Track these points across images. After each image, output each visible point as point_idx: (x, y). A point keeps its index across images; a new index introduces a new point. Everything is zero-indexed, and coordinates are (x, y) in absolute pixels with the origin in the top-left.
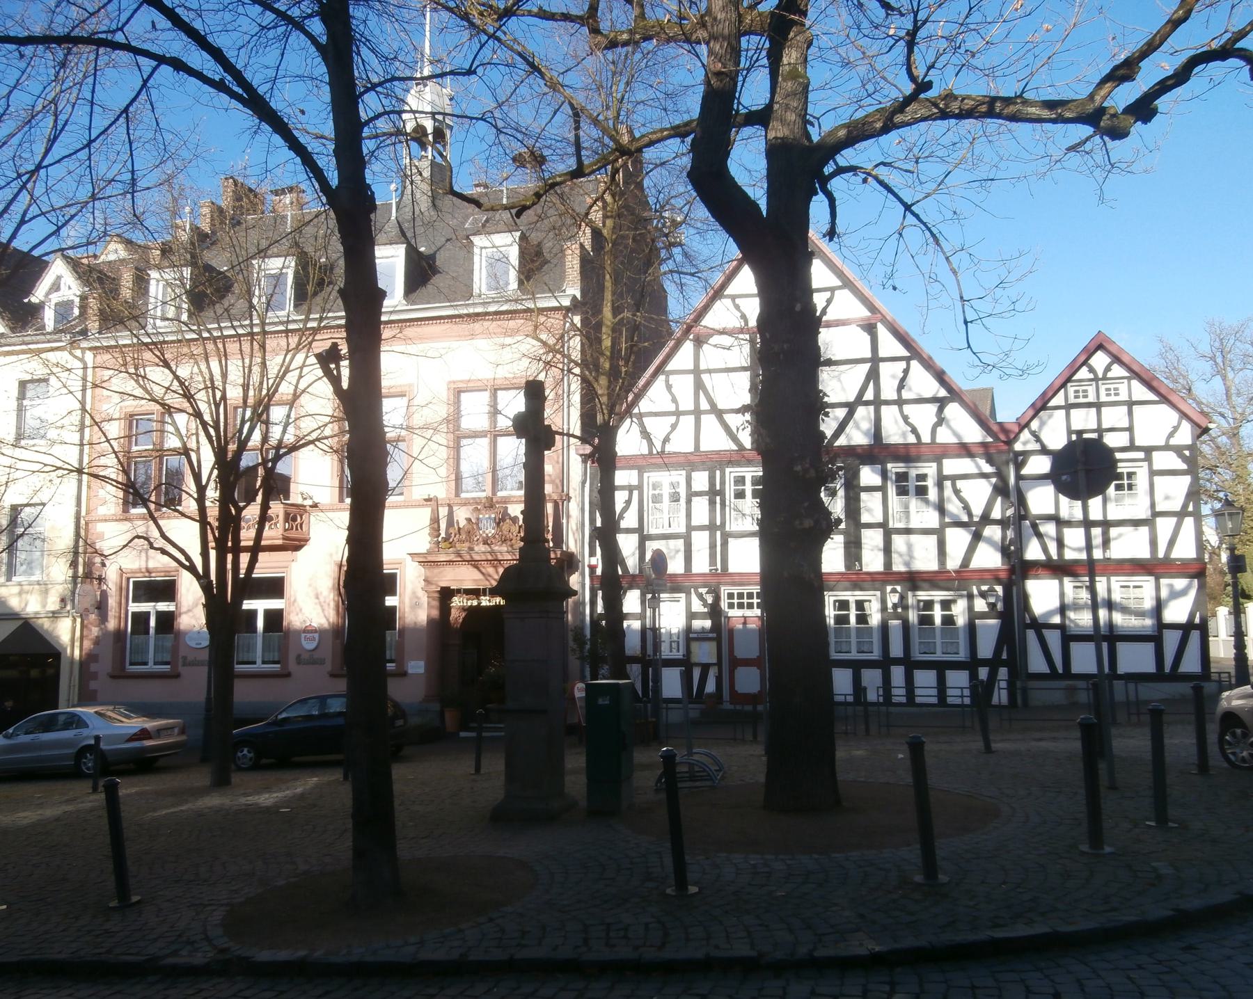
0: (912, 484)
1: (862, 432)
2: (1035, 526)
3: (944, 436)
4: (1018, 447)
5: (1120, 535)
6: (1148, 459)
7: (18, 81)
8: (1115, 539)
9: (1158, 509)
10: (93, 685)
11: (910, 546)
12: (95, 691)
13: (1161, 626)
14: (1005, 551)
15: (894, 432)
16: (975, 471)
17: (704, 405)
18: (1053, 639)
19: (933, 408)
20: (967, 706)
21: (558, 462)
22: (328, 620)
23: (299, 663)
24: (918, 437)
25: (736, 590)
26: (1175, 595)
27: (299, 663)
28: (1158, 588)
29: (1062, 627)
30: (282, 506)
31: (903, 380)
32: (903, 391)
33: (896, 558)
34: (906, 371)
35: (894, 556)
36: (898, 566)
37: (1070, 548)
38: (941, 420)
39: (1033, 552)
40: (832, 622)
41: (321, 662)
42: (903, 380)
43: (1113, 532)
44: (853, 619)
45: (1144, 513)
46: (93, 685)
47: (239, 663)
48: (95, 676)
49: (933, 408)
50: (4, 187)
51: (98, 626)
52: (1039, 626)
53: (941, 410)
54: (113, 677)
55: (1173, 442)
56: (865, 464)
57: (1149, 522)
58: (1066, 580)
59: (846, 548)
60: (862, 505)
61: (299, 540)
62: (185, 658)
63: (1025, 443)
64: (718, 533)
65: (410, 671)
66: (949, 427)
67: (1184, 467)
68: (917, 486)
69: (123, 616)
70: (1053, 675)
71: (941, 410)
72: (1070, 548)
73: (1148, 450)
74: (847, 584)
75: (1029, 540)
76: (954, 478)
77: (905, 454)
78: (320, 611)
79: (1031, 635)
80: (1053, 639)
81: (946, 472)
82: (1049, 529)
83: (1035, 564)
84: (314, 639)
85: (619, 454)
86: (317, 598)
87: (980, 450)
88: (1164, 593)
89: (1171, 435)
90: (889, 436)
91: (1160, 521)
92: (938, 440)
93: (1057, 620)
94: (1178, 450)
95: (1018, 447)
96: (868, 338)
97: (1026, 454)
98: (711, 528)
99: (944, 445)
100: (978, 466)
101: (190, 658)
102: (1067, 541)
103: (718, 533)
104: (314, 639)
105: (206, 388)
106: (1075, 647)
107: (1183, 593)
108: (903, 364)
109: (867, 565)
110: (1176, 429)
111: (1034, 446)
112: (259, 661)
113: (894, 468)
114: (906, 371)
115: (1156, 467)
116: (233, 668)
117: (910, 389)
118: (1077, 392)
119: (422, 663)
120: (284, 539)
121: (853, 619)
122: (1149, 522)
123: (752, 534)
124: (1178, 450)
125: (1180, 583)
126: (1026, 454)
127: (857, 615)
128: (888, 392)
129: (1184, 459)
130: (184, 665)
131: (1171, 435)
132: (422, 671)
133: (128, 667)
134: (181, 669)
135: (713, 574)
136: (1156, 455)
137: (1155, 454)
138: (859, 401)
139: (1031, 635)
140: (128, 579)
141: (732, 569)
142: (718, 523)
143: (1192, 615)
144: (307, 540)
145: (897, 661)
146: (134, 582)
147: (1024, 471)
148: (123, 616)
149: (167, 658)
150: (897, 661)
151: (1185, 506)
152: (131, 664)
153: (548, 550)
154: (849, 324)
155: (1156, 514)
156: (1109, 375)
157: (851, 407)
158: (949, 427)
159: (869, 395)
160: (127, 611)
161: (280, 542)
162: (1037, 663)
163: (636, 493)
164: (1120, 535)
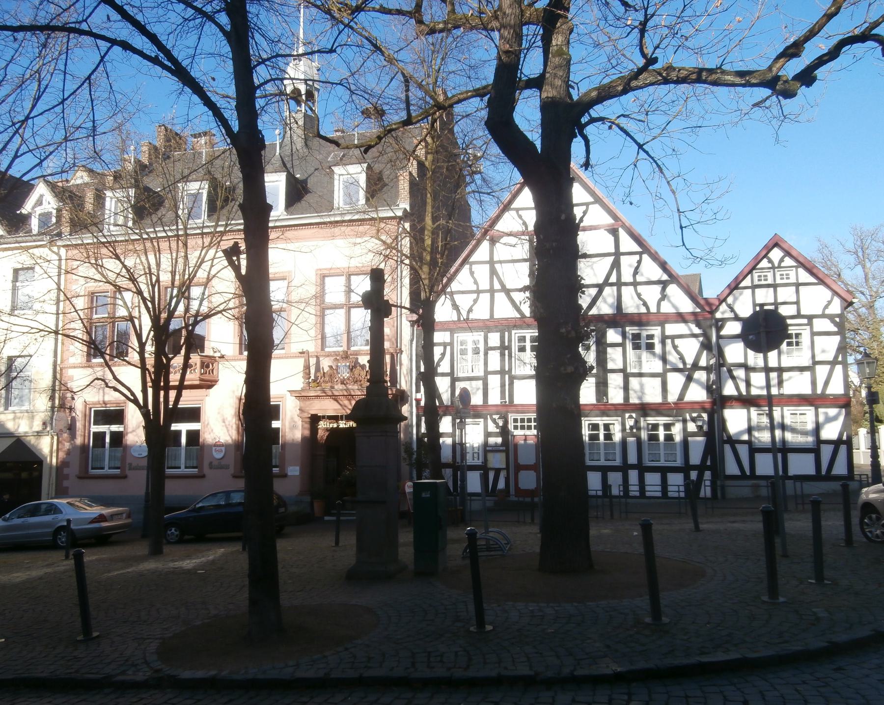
0: (643, 341)
1: (608, 305)
2: (730, 371)
3: (666, 308)
4: (718, 315)
5: (790, 378)
6: (810, 324)
7: (13, 57)
8: (787, 380)
9: (817, 359)
10: (66, 483)
11: (642, 386)
12: (67, 488)
13: (819, 442)
14: (709, 389)
15: (631, 305)
16: (688, 332)
17: (497, 286)
18: (743, 451)
19: (658, 288)
20: (682, 498)
21: (394, 326)
22: (231, 438)
23: (211, 468)
24: (648, 308)
25: (519, 417)
26: (829, 420)
27: (211, 468)
28: (817, 415)
29: (749, 443)
30: (199, 357)
31: (637, 268)
32: (637, 276)
33: (632, 394)
34: (639, 262)
35: (631, 392)
36: (634, 400)
37: (755, 387)
38: (664, 297)
39: (729, 389)
40: (587, 439)
41: (227, 467)
42: (637, 268)
43: (786, 375)
44: (602, 437)
45: (807, 362)
46: (66, 483)
47: (169, 468)
48: (67, 477)
49: (658, 288)
50: (2, 132)
51: (69, 442)
52: (733, 442)
53: (664, 289)
54: (80, 478)
55: (827, 312)
56: (610, 327)
57: (810, 369)
58: (752, 409)
59: (597, 387)
60: (608, 356)
61: (211, 381)
62: (130, 464)
63: (723, 313)
64: (507, 376)
65: (289, 474)
66: (670, 301)
67: (836, 329)
68: (647, 343)
69: (86, 434)
70: (743, 476)
71: (664, 289)
72: (755, 387)
73: (810, 318)
74: (598, 412)
75: (726, 381)
76: (673, 338)
77: (639, 320)
78: (226, 431)
79: (727, 448)
80: (743, 451)
81: (667, 333)
82: (740, 373)
83: (730, 398)
84: (221, 451)
85: (437, 320)
86: (224, 422)
87: (692, 318)
88: (821, 419)
89: (826, 307)
90: (627, 308)
91: (818, 368)
92: (662, 311)
93: (745, 437)
94: (831, 318)
95: (718, 315)
96: (613, 238)
97: (724, 321)
98: (502, 372)
99: (666, 314)
100: (690, 329)
101: (134, 464)
102: (753, 382)
103: (507, 376)
104: (221, 451)
105: (146, 274)
106: (759, 457)
107: (835, 418)
108: (637, 257)
109: (612, 399)
110: (829, 303)
111: (729, 315)
112: (183, 466)
113: (630, 330)
114: (639, 262)
115: (815, 330)
116: (164, 471)
117: (642, 275)
118: (759, 276)
119: (298, 468)
120: (200, 380)
121: (602, 437)
122: (810, 369)
123: (530, 377)
124: (831, 318)
125: (833, 412)
126: (724, 321)
127: (605, 434)
128: (627, 277)
129: (836, 324)
130: (130, 470)
131: (826, 307)
132: (298, 473)
133: (90, 470)
134: (128, 472)
135: (503, 405)
136: (815, 321)
137: (815, 320)
138: (606, 283)
139: (727, 448)
140: (90, 409)
141: (516, 402)
142: (507, 369)
143: (841, 434)
144: (216, 381)
145: (633, 467)
146: (95, 411)
147: (723, 333)
148: (86, 434)
149: (118, 464)
150: (633, 467)
151: (836, 357)
152: (93, 469)
153: (387, 388)
154: (599, 228)
155: (815, 363)
156: (783, 264)
157: (601, 287)
158: (670, 301)
159: (613, 279)
160: (89, 431)
161: (197, 382)
162: (731, 468)
163: (448, 348)
164: (790, 378)
